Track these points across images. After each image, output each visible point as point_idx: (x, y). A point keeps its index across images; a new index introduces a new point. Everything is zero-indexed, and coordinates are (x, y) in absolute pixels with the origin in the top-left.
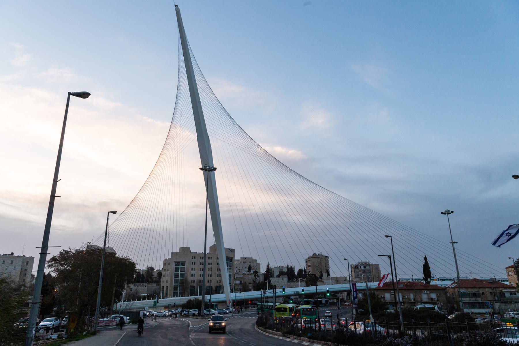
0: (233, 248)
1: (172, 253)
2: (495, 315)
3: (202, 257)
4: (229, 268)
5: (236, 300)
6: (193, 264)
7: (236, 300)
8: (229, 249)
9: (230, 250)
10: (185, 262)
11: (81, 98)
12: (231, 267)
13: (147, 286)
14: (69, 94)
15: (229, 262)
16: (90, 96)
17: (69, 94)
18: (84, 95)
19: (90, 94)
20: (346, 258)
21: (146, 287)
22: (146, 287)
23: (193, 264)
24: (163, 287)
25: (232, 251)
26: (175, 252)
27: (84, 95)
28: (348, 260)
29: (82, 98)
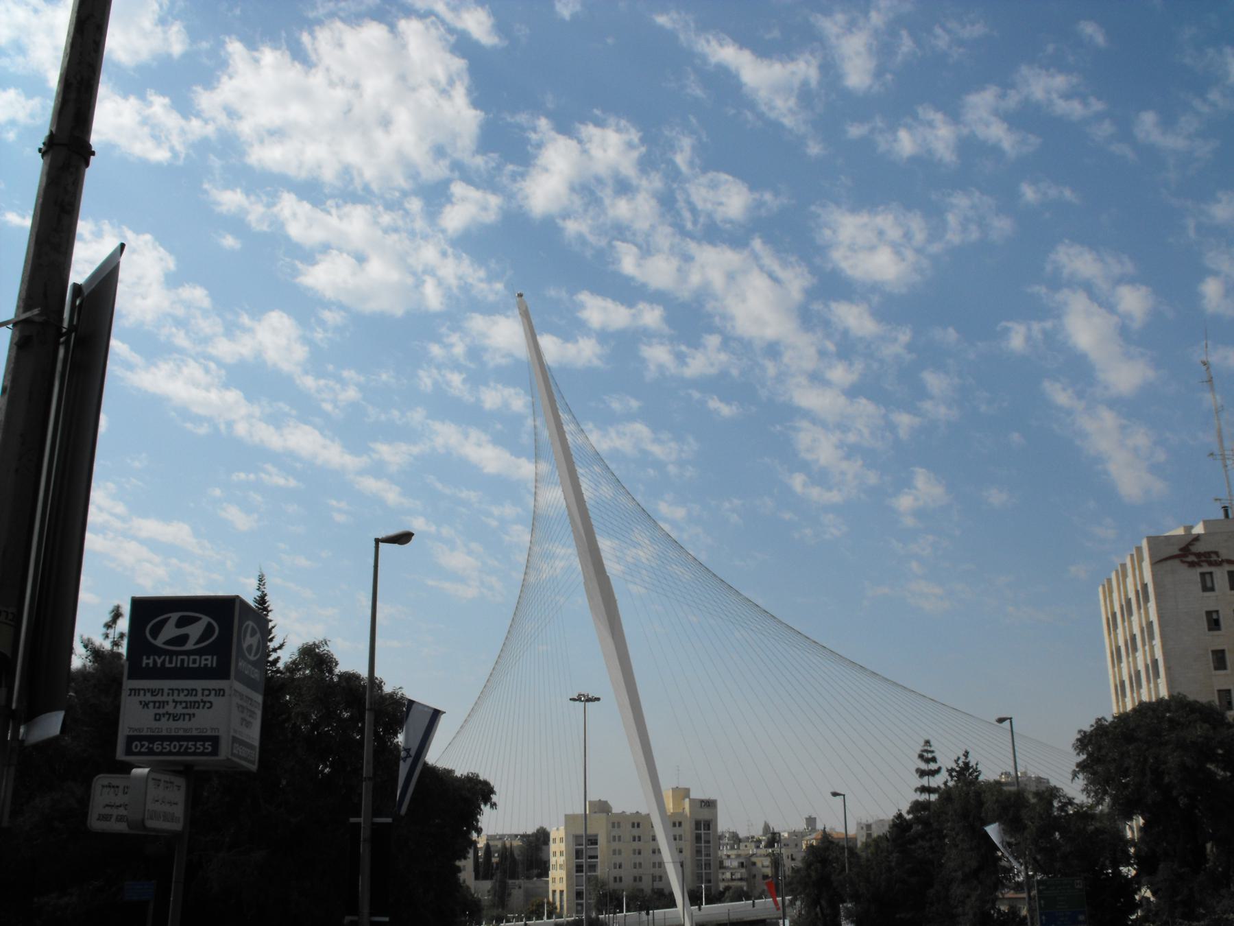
0: (712, 798)
1: (566, 816)
2: (215, 657)
3: (617, 842)
4: (705, 833)
5: (704, 821)
6: (617, 839)
7: (704, 821)
8: (702, 801)
9: (703, 804)
10: (596, 836)
11: (396, 545)
12: (708, 842)
13: (522, 886)
14: (377, 541)
15: (702, 832)
16: (413, 538)
17: (377, 541)
18: (403, 538)
19: (413, 534)
20: (839, 791)
21: (520, 887)
22: (520, 887)
23: (617, 839)
24: (554, 892)
25: (709, 804)
26: (571, 813)
27: (403, 538)
28: (844, 795)
29: (399, 544)
